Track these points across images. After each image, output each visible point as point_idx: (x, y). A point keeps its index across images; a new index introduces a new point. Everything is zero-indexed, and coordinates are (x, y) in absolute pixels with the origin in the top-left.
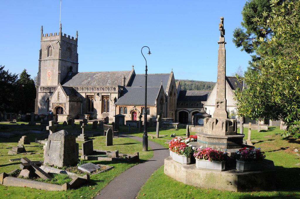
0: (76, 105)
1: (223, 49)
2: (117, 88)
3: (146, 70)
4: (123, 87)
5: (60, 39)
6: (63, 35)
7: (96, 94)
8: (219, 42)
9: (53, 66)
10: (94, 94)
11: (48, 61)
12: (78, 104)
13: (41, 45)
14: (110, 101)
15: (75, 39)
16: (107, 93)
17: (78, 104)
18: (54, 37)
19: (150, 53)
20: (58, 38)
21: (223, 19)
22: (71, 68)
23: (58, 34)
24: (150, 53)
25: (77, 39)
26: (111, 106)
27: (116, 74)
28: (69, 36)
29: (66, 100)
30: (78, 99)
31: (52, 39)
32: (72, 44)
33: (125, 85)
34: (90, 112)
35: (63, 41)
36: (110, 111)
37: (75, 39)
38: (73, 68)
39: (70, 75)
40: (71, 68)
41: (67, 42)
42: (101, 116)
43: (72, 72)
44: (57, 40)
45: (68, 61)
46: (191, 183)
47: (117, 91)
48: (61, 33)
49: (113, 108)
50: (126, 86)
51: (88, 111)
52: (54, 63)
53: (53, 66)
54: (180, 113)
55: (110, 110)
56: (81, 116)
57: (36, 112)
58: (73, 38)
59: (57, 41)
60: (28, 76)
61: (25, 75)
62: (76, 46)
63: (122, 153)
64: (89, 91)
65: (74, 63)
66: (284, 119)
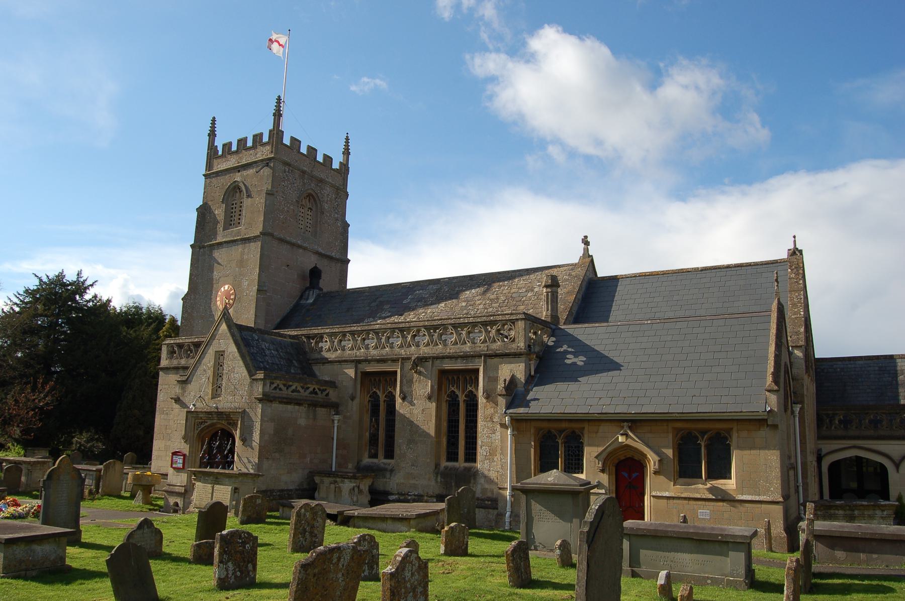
0: (302, 422)
3: (278, 115)
4: (551, 326)
9: (241, 263)
12: (315, 418)
14: (481, 400)
15: (336, 165)
16: (466, 357)
17: (315, 418)
21: (794, 237)
22: (315, 274)
25: (345, 167)
26: (490, 424)
28: (312, 151)
29: (250, 393)
30: (314, 392)
31: (244, 162)
32: (321, 181)
33: (555, 318)
34: (375, 460)
37: (336, 165)
38: (323, 276)
39: (311, 301)
40: (315, 274)
41: (304, 172)
42: (433, 483)
43: (321, 289)
45: (305, 249)
46: (493, 494)
50: (563, 316)
51: (366, 454)
53: (241, 263)
54: (835, 467)
55: (481, 452)
56: (327, 480)
58: (328, 159)
62: (342, 193)
64: (374, 353)
65: (330, 258)
66: (22, 436)
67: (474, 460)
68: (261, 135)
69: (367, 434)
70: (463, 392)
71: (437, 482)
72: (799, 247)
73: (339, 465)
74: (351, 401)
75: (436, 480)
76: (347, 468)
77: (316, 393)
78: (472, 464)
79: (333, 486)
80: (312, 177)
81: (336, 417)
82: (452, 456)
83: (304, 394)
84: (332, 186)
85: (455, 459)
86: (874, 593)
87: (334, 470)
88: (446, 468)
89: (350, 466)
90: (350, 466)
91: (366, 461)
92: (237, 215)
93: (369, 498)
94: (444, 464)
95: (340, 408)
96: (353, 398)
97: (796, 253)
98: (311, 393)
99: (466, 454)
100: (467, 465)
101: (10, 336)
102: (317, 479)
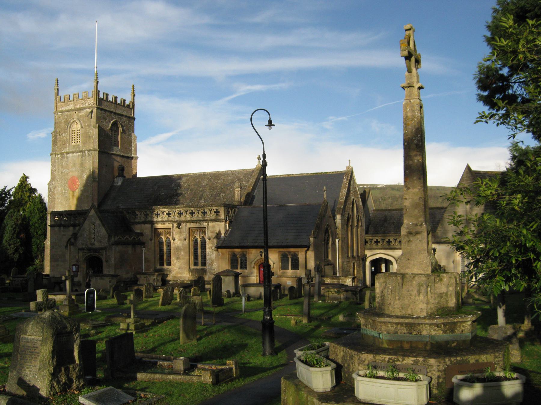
1: (415, 101)
2: (222, 210)
5: (95, 105)
6: (101, 96)
7: (175, 225)
8: (404, 84)
10: (170, 226)
11: (71, 155)
13: (55, 120)
14: (207, 241)
15: (127, 103)
18: (82, 101)
19: (270, 124)
20: (92, 102)
21: (350, 161)
23: (90, 96)
24: (270, 124)
25: (133, 103)
26: (211, 250)
27: (222, 178)
31: (78, 107)
32: (121, 115)
35: (102, 109)
36: (207, 264)
42: (188, 275)
44: (89, 108)
47: (222, 216)
48: (98, 92)
49: (214, 256)
51: (158, 264)
52: (83, 158)
55: (208, 262)
56: (142, 277)
57: (504, 307)
59: (89, 110)
60: (34, 190)
61: (366, 255)
63: (85, 108)
67: (205, 265)
68: (479, 95)
69: (158, 256)
70: (200, 237)
71: (190, 275)
72: (351, 165)
73: (146, 269)
74: (150, 242)
75: (189, 274)
76: (150, 271)
77: (135, 239)
78: (162, 267)
79: (145, 279)
80: (116, 114)
81: (144, 249)
82: (196, 264)
83: (131, 239)
84: (127, 117)
85: (163, 265)
86: (207, 311)
87: (144, 271)
88: (193, 269)
89: (151, 270)
90: (151, 270)
91: (158, 267)
92: (76, 140)
93: (161, 283)
94: (192, 267)
95: (146, 245)
96: (151, 240)
97: (24, 174)
98: (133, 239)
99: (202, 263)
100: (202, 267)
101: (156, 214)
102: (138, 276)
